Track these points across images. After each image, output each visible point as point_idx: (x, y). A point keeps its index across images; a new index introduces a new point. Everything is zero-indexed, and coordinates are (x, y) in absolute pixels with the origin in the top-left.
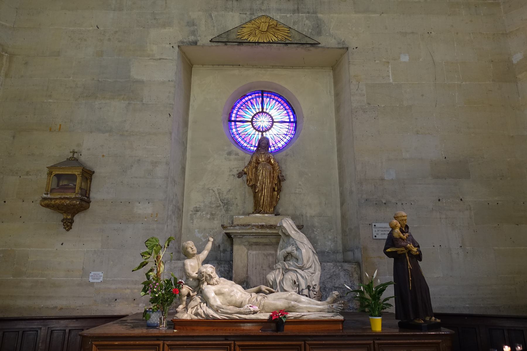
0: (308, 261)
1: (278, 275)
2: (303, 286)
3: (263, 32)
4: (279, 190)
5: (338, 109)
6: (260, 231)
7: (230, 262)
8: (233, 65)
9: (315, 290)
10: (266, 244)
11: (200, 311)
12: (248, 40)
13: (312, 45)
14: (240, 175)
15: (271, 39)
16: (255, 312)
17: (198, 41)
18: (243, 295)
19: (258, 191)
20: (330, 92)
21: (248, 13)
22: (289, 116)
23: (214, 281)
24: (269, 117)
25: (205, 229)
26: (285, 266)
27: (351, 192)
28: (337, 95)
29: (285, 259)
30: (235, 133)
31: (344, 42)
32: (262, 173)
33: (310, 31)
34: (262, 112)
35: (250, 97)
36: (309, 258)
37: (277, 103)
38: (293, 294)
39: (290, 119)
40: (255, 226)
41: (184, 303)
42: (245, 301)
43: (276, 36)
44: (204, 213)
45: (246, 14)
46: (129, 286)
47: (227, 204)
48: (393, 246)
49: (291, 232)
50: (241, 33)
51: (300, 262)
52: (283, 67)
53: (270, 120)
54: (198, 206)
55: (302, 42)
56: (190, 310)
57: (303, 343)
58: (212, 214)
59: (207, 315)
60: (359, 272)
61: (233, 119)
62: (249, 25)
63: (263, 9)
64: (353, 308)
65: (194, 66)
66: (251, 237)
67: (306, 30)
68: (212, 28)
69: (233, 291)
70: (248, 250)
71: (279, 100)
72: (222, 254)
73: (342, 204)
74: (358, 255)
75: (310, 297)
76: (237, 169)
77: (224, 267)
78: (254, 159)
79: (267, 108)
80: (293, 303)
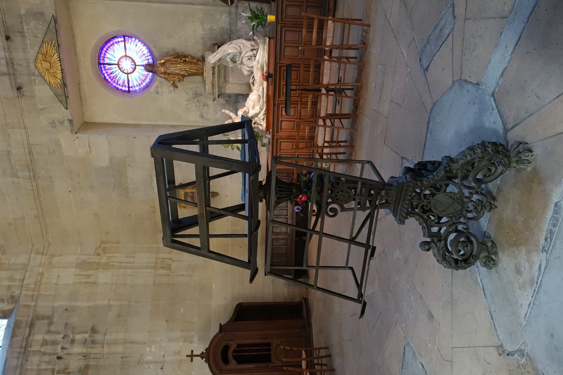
0: (237, 49)
1: (245, 68)
2: (251, 53)
3: (51, 65)
4: (185, 56)
6: (216, 75)
7: (237, 95)
8: (80, 89)
9: (254, 44)
11: (262, 118)
12: (61, 79)
13: (56, 22)
14: (175, 86)
15: (57, 59)
16: (263, 89)
17: (68, 119)
18: (255, 94)
19: (187, 73)
21: (33, 78)
22: (119, 42)
23: (247, 110)
24: (121, 59)
30: (139, 87)
32: (173, 70)
33: (41, 23)
34: (118, 64)
35: (106, 75)
36: (234, 47)
37: (108, 51)
38: (255, 63)
39: (122, 41)
40: (213, 79)
41: (258, 126)
42: (258, 93)
43: (53, 54)
44: (203, 111)
45: (34, 80)
47: (197, 95)
49: (218, 57)
50: (55, 84)
51: (237, 54)
52: (74, 46)
54: (199, 115)
55: (55, 32)
56: (262, 123)
57: (279, 64)
58: (204, 106)
59: (264, 114)
61: (127, 89)
62: (47, 77)
63: (26, 65)
64: (268, 9)
65: (85, 121)
66: (220, 81)
67: (40, 27)
69: (252, 100)
70: (229, 83)
71: (105, 49)
72: (232, 98)
75: (258, 49)
76: (169, 87)
77: (240, 99)
78: (163, 76)
80: (259, 66)
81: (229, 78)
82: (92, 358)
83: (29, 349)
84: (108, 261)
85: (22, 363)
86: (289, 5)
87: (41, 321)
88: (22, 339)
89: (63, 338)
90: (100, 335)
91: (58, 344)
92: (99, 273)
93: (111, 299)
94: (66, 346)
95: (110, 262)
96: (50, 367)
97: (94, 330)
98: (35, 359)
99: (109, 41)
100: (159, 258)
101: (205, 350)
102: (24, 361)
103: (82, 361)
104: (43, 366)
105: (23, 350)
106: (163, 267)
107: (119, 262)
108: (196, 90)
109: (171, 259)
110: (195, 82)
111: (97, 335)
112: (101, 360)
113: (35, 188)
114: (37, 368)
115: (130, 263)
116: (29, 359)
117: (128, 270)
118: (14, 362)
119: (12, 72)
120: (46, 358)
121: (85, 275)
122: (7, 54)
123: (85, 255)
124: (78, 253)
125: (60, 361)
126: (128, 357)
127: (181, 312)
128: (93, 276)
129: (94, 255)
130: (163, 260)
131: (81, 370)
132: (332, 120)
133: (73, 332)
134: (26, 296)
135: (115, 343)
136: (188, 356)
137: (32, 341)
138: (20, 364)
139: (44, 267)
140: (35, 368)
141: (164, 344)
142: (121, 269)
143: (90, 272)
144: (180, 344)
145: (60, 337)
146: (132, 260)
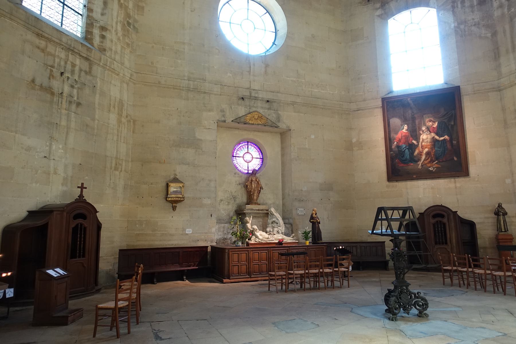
5: (283, 155)
6: (258, 212)
10: (259, 217)
13: (276, 127)
16: (273, 240)
20: (279, 146)
21: (248, 108)
25: (225, 209)
26: (273, 226)
27: (289, 195)
28: (283, 149)
29: (272, 223)
31: (289, 126)
34: (248, 152)
45: (247, 108)
46: (203, 235)
47: (235, 198)
48: (313, 219)
53: (251, 157)
60: (291, 228)
62: (249, 115)
67: (273, 119)
68: (232, 114)
71: (256, 147)
73: (283, 199)
74: (291, 221)
79: (250, 151)
81: (255, 219)
82: (59, 100)
83: (70, 52)
84: (123, 123)
85: (62, 45)
86: (315, 252)
87: (88, 66)
88: (80, 50)
89: (75, 80)
90: (75, 109)
91: (72, 75)
92: (116, 115)
93: (99, 121)
94: (69, 80)
95: (122, 124)
96: (56, 65)
97: (79, 104)
98: (63, 55)
99: (260, 149)
100: (122, 162)
101: (85, 199)
102: (63, 47)
103: (57, 91)
104: (57, 60)
105: (72, 48)
106: (116, 165)
107: (121, 131)
108: (237, 198)
109: (121, 171)
110: (242, 197)
111: (75, 107)
112: (57, 107)
113: (181, 88)
114: (56, 55)
115: (121, 139)
116: (63, 51)
117: (116, 137)
118: (64, 40)
119: (251, 98)
120: (62, 63)
121: (115, 104)
122: (260, 99)
123: (127, 107)
124: (128, 102)
125: (59, 74)
126: (57, 128)
127: (86, 177)
128: (114, 110)
129: (127, 113)
130: (121, 165)
131: (51, 89)
132: (111, 311)
133: (79, 88)
134: (107, 60)
135: (68, 120)
136: (82, 184)
137: (76, 56)
138: (62, 43)
139: (123, 77)
140: (57, 54)
141: (63, 160)
142: (117, 132)
143: (116, 108)
144: (62, 175)
145: (76, 77)
146: (122, 141)
